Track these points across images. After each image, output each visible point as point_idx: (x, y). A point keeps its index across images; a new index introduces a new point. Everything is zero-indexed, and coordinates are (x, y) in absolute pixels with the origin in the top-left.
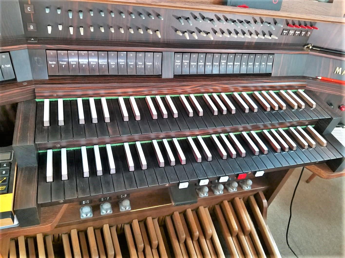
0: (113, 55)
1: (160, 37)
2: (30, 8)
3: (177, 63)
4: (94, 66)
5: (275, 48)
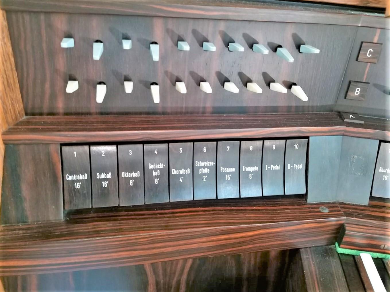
1: (304, 98)
2: (372, 51)
4: (182, 179)
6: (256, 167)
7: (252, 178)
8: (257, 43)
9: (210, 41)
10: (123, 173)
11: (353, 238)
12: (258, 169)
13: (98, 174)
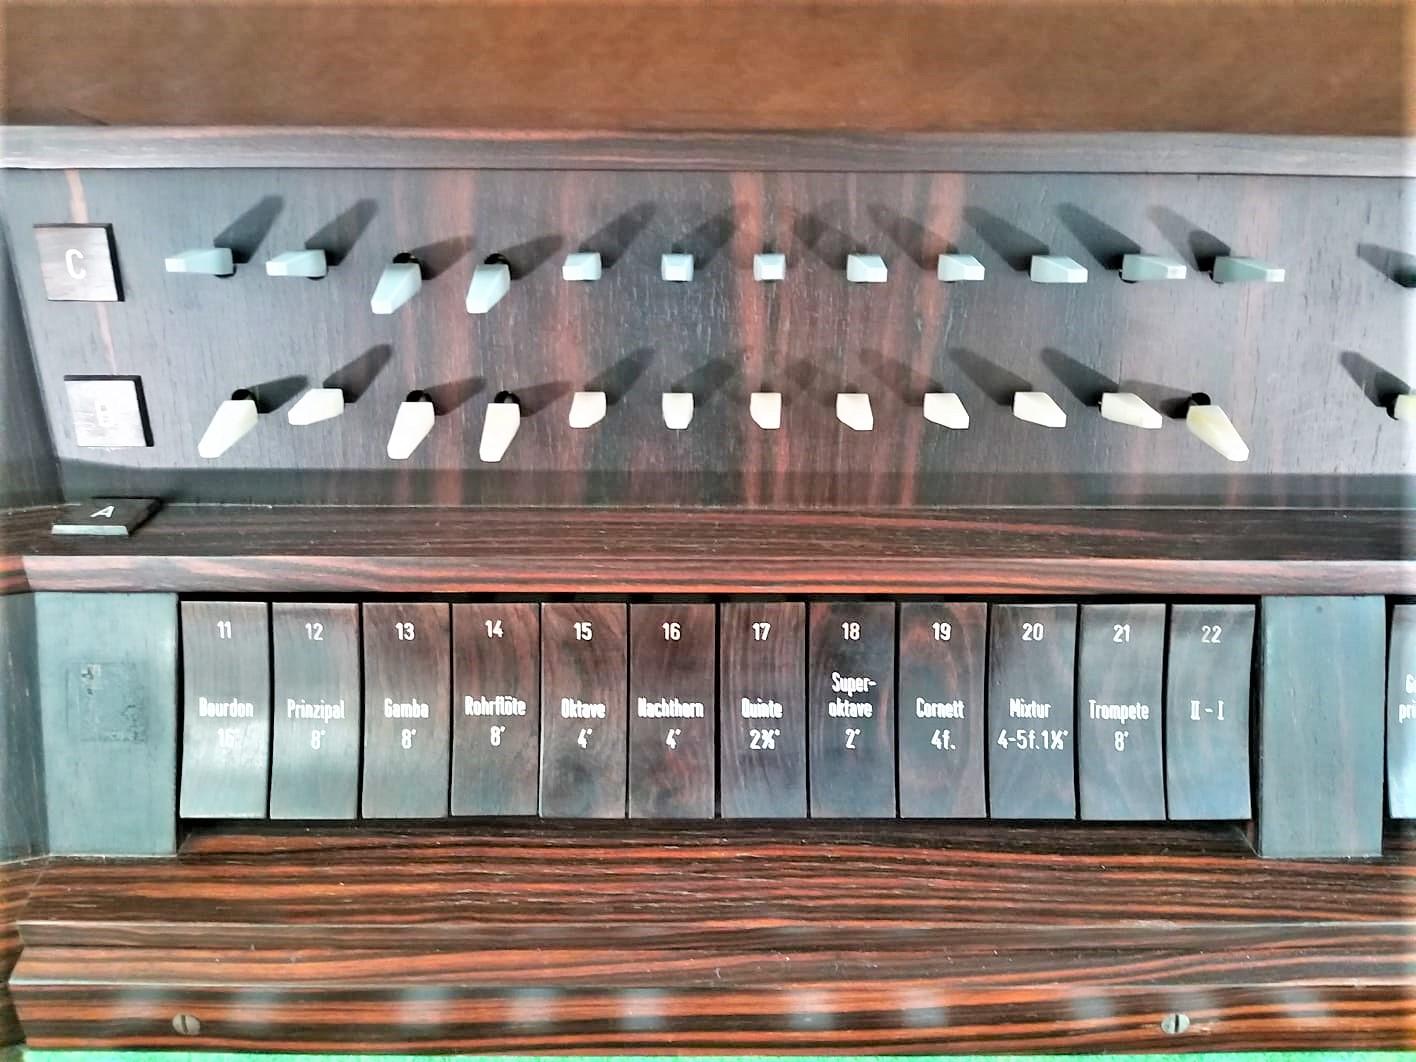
6: (1138, 704)
8: (1136, 250)
9: (1051, 252)
10: (565, 701)
12: (1147, 712)
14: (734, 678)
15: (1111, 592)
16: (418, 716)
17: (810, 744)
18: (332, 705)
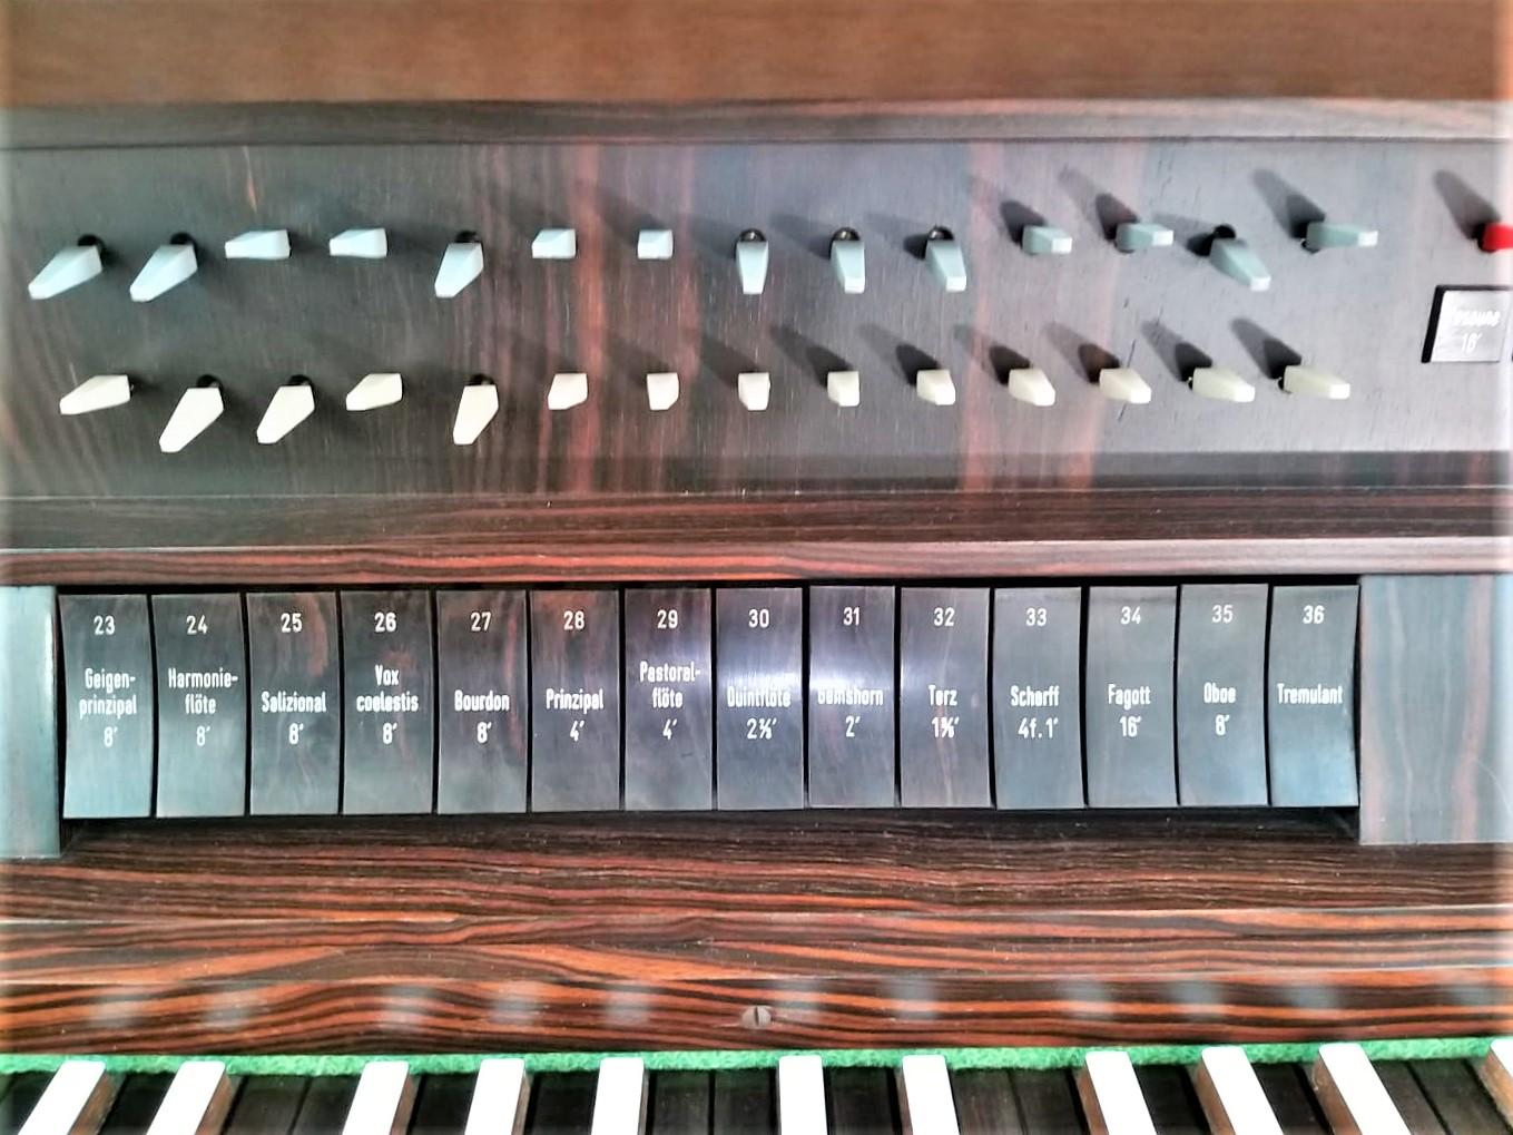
0: (759, 618)
3: (101, 693)
5: (1311, 512)
7: (1226, 730)
8: (1040, 222)
11: (420, 1026)
13: (1015, 689)
14: (261, 668)
15: (1130, 574)
16: (497, 708)
17: (527, 729)
18: (314, 697)
